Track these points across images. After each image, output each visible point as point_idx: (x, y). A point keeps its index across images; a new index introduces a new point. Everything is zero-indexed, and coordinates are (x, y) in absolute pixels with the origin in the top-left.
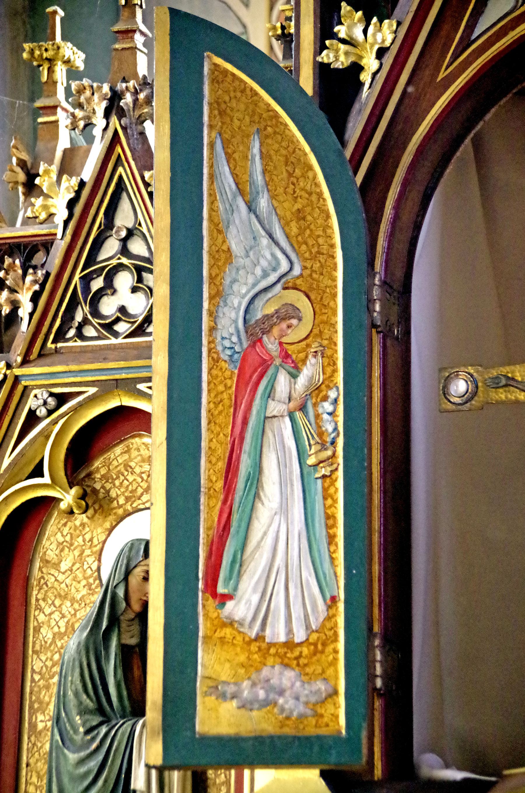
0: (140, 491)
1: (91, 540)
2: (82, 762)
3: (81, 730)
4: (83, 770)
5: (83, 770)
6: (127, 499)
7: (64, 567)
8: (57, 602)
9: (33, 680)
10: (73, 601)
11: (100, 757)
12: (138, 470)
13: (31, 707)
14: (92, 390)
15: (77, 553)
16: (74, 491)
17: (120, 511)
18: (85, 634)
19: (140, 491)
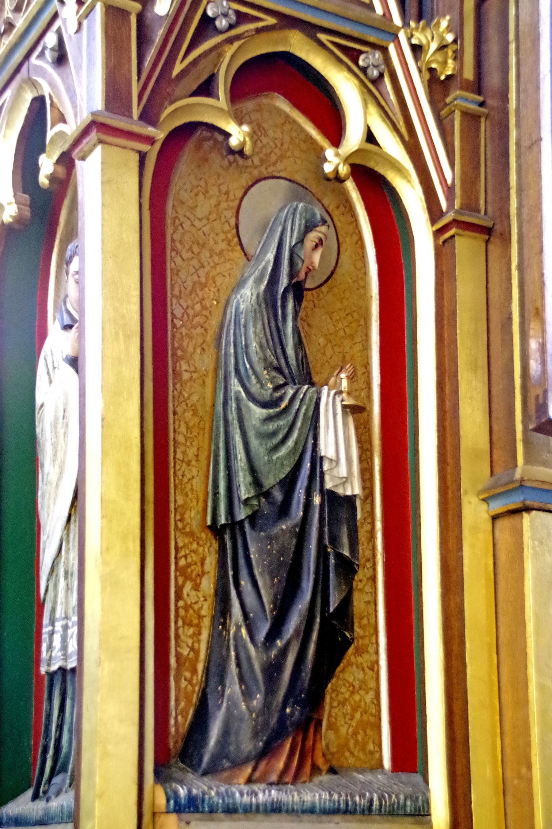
0: (273, 158)
1: (227, 193)
2: (269, 419)
3: (270, 386)
4: (272, 426)
5: (272, 426)
6: (262, 161)
7: (200, 212)
8: (196, 249)
9: (174, 326)
10: (212, 251)
11: (291, 418)
12: (271, 133)
13: (174, 354)
14: (271, 21)
15: (213, 202)
16: (246, 128)
17: (256, 172)
18: (263, 287)
19: (273, 158)
